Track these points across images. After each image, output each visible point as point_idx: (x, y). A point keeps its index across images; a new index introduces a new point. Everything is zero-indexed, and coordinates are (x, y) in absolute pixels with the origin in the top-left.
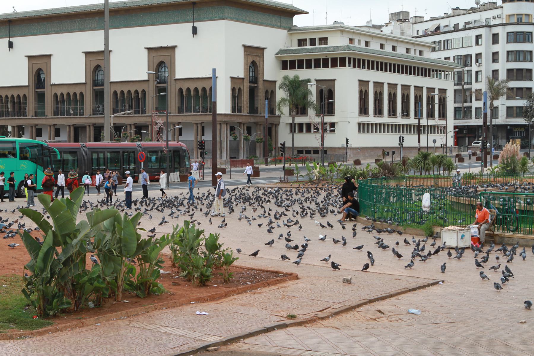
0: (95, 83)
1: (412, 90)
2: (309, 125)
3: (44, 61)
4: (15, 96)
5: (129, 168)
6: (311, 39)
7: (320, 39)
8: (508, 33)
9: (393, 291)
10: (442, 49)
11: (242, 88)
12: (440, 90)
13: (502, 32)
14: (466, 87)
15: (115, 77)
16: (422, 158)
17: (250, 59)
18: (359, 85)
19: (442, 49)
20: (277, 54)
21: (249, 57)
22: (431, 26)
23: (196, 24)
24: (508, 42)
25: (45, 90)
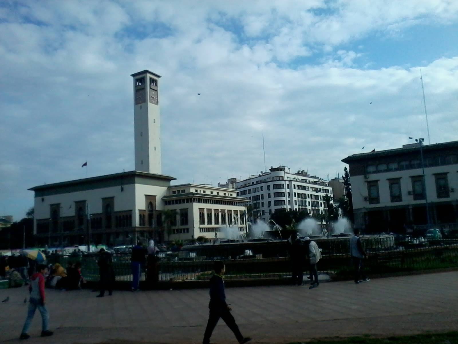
1: (233, 212)
2: (177, 230)
5: (129, 249)
6: (178, 191)
7: (182, 191)
10: (248, 193)
12: (228, 210)
13: (271, 184)
14: (258, 210)
17: (149, 201)
18: (199, 210)
19: (248, 193)
20: (163, 198)
22: (243, 184)
23: (123, 186)
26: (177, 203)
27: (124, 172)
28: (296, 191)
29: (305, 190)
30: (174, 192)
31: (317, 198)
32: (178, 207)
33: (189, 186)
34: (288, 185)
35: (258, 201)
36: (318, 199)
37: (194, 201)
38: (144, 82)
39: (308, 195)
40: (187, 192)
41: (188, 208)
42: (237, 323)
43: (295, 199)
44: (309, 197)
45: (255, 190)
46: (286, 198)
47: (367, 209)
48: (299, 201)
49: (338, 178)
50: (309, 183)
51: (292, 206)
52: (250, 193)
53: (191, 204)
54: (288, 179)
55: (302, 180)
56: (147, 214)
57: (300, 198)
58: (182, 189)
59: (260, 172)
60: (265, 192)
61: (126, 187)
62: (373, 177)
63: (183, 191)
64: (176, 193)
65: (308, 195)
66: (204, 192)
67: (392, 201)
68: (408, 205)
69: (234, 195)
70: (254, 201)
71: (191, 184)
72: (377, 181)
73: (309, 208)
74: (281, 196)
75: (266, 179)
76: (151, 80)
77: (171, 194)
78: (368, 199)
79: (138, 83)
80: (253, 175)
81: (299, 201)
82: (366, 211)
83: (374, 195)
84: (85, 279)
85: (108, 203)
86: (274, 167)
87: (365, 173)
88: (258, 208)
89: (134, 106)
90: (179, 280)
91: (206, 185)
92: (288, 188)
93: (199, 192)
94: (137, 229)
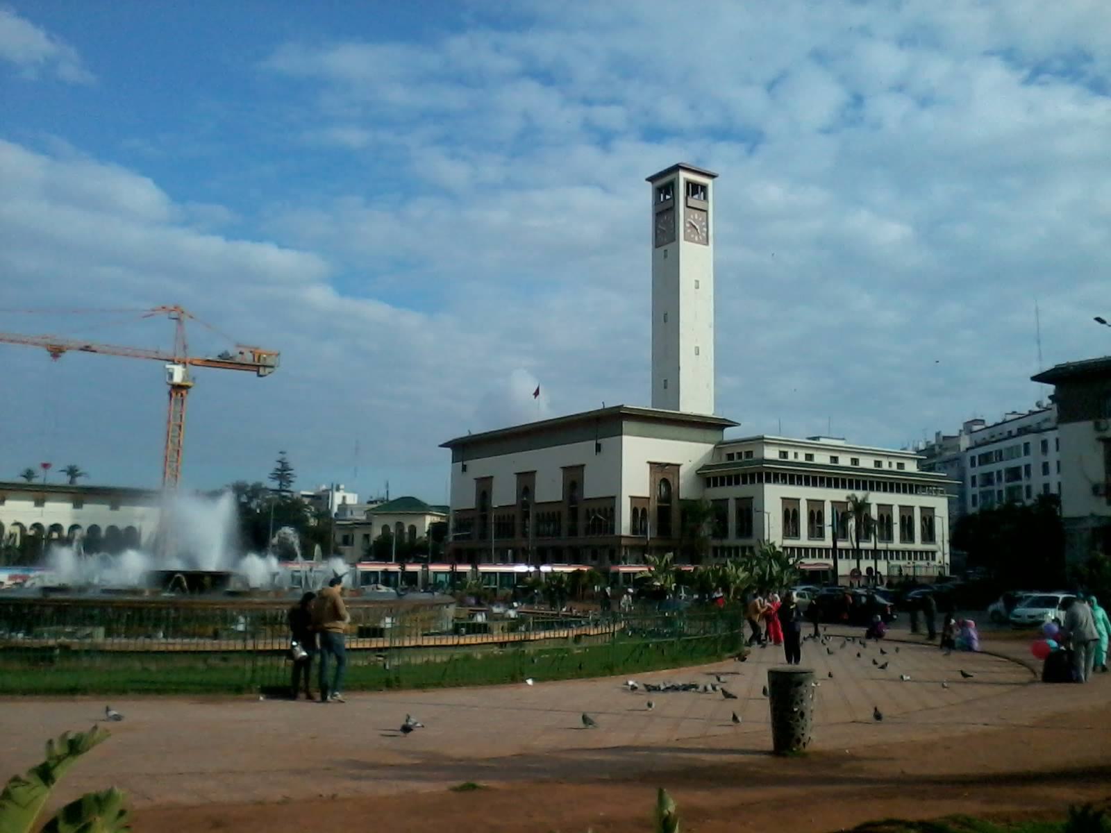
9: (724, 727)
11: (647, 508)
15: (587, 494)
16: (889, 585)
17: (660, 476)
26: (730, 484)
27: (604, 409)
28: (979, 471)
30: (730, 456)
32: (731, 493)
33: (761, 441)
37: (768, 481)
40: (755, 456)
41: (752, 498)
47: (1100, 518)
49: (386, 498)
53: (760, 485)
56: (653, 507)
58: (747, 450)
59: (1034, 405)
60: (1034, 459)
61: (604, 442)
63: (749, 454)
64: (733, 459)
66: (809, 457)
69: (911, 467)
71: (765, 436)
76: (690, 185)
77: (724, 460)
78: (1102, 491)
80: (1014, 413)
82: (1096, 525)
85: (573, 477)
89: (653, 249)
90: (657, 643)
91: (822, 441)
93: (791, 458)
94: (623, 542)
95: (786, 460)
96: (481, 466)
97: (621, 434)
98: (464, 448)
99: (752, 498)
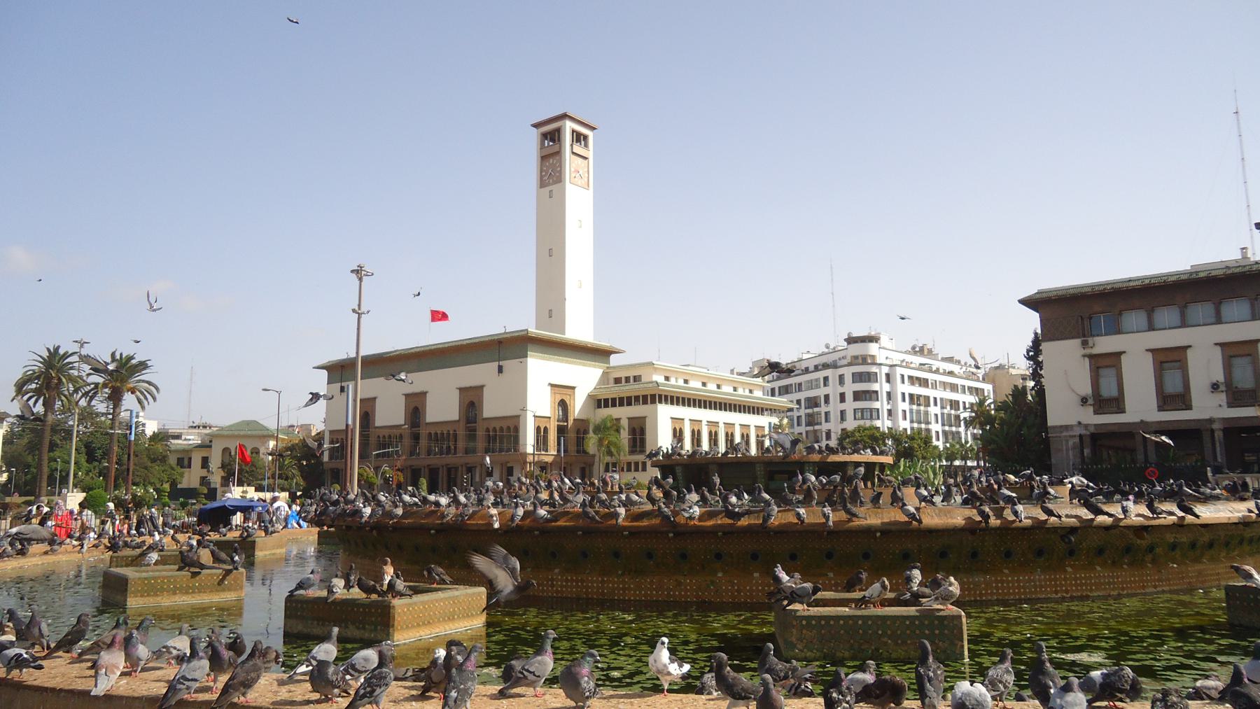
0: (468, 421)
3: (569, 391)
4: (381, 436)
6: (626, 378)
8: (853, 374)
11: (548, 427)
13: (848, 372)
15: (378, 423)
17: (559, 398)
18: (672, 422)
19: (794, 391)
21: (557, 395)
23: (501, 363)
24: (853, 382)
25: (557, 423)
27: (505, 333)
28: (908, 389)
29: (927, 386)
31: (957, 407)
34: (888, 376)
35: (816, 410)
36: (959, 409)
37: (660, 402)
38: (559, 140)
39: (935, 399)
42: (1115, 378)
43: (905, 406)
44: (936, 404)
45: (812, 385)
46: (882, 405)
47: (1086, 426)
48: (912, 412)
50: (937, 371)
51: (894, 421)
52: (800, 390)
54: (888, 362)
55: (921, 364)
57: (914, 404)
59: (824, 347)
60: (833, 390)
62: (1105, 344)
65: (935, 399)
67: (1161, 408)
68: (1211, 421)
70: (809, 408)
71: (654, 362)
72: (1118, 355)
73: (936, 427)
74: (871, 399)
75: (836, 360)
79: (546, 141)
81: (911, 411)
83: (1108, 390)
84: (1110, 452)
85: (471, 400)
86: (855, 335)
87: (1084, 332)
88: (817, 424)
89: (537, 190)
92: (888, 380)
95: (688, 385)
96: (364, 387)
97: (527, 357)
98: (340, 371)
99: (645, 417)
